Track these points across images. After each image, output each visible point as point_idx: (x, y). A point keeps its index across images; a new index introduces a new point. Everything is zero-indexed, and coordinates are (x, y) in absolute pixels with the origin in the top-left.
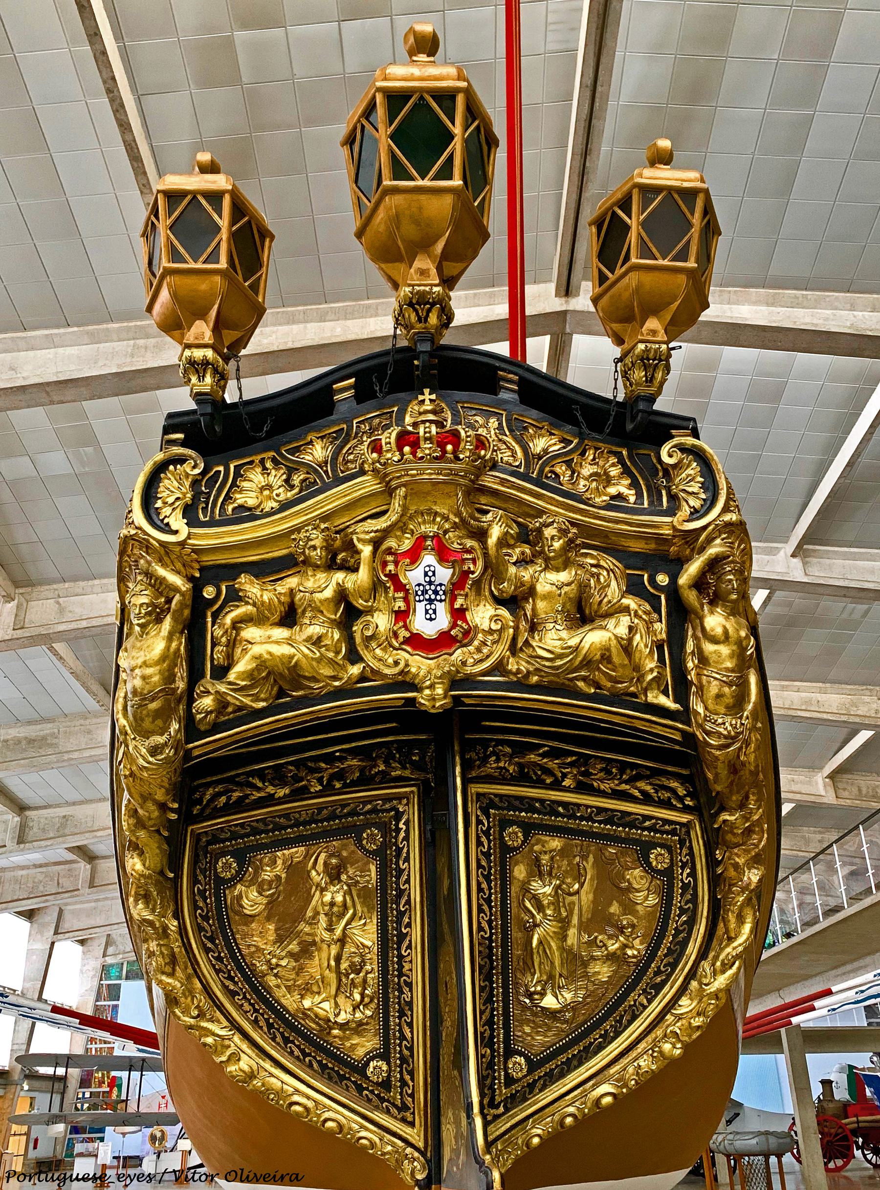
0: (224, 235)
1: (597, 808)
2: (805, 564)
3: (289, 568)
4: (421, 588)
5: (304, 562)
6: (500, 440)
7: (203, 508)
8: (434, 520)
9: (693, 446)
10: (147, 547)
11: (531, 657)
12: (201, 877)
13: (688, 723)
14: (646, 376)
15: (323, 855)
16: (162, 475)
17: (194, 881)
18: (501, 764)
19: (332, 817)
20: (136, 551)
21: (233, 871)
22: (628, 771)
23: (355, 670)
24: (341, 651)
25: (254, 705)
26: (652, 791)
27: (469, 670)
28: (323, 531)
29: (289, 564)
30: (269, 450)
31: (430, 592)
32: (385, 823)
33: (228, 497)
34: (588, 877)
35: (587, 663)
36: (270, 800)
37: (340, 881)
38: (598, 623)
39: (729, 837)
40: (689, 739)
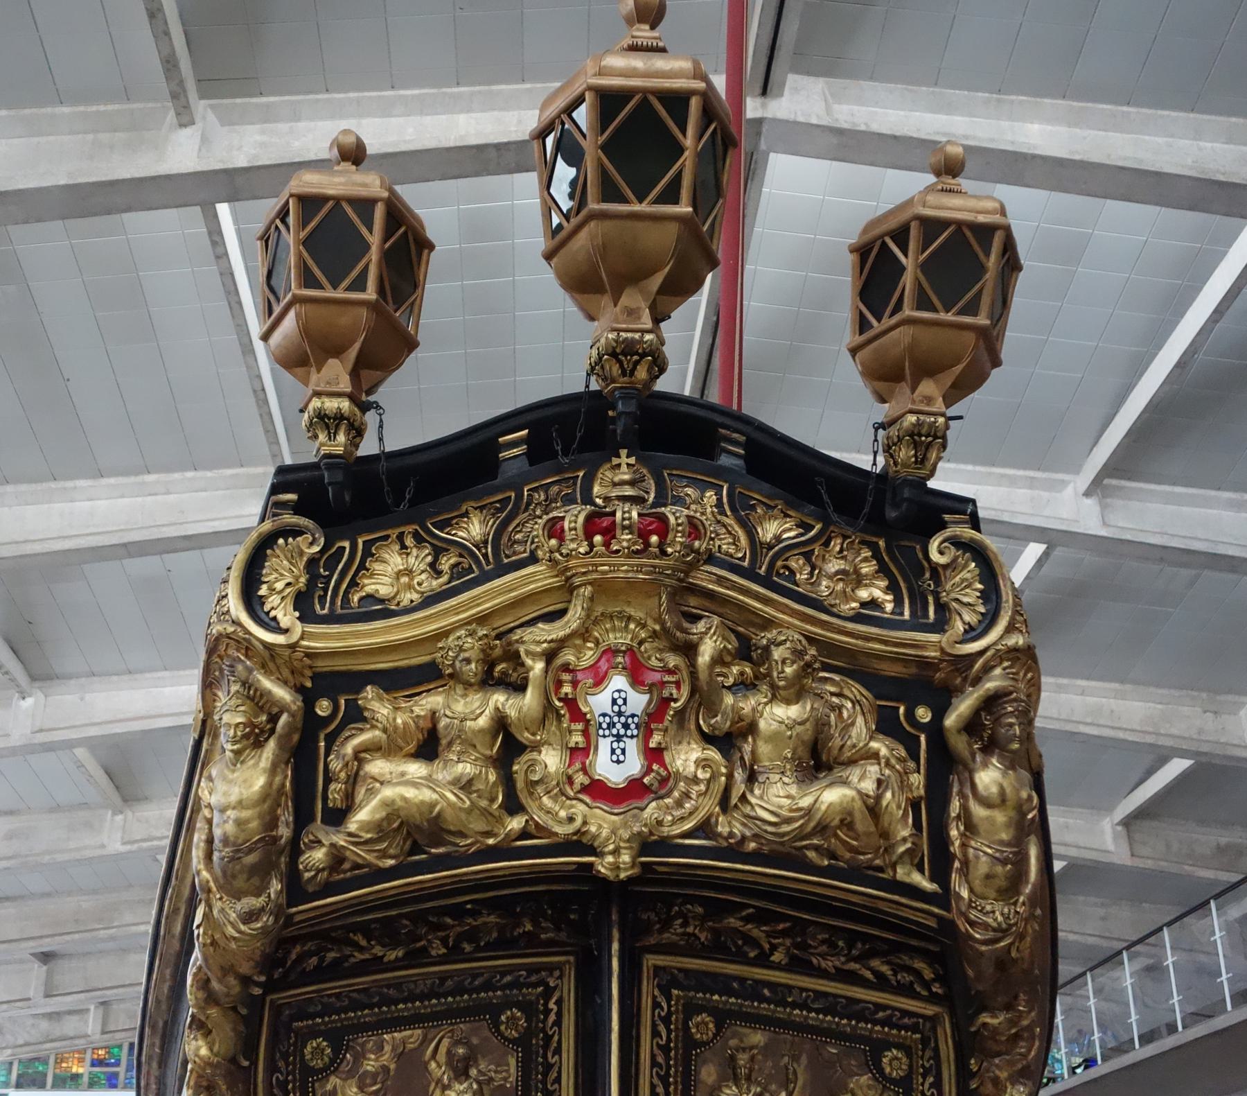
0: (374, 255)
1: (814, 991)
2: (1104, 507)
3: (429, 681)
4: (607, 719)
5: (451, 676)
6: (719, 522)
7: (320, 597)
8: (627, 626)
9: (972, 540)
10: (247, 648)
11: (747, 816)
12: (281, 1064)
13: (948, 908)
14: (915, 456)
15: (446, 1042)
16: (269, 552)
17: (272, 1068)
18: (690, 930)
19: (459, 990)
20: (230, 652)
21: (326, 1059)
22: (859, 945)
23: (515, 823)
24: (497, 797)
25: (381, 864)
26: (889, 973)
27: (665, 831)
28: (480, 639)
29: (427, 676)
30: (413, 523)
31: (619, 726)
32: (531, 1003)
33: (354, 584)
34: (800, 1083)
35: (822, 828)
36: (376, 964)
37: (468, 1077)
38: (839, 773)
39: (990, 1044)
40: (947, 927)
